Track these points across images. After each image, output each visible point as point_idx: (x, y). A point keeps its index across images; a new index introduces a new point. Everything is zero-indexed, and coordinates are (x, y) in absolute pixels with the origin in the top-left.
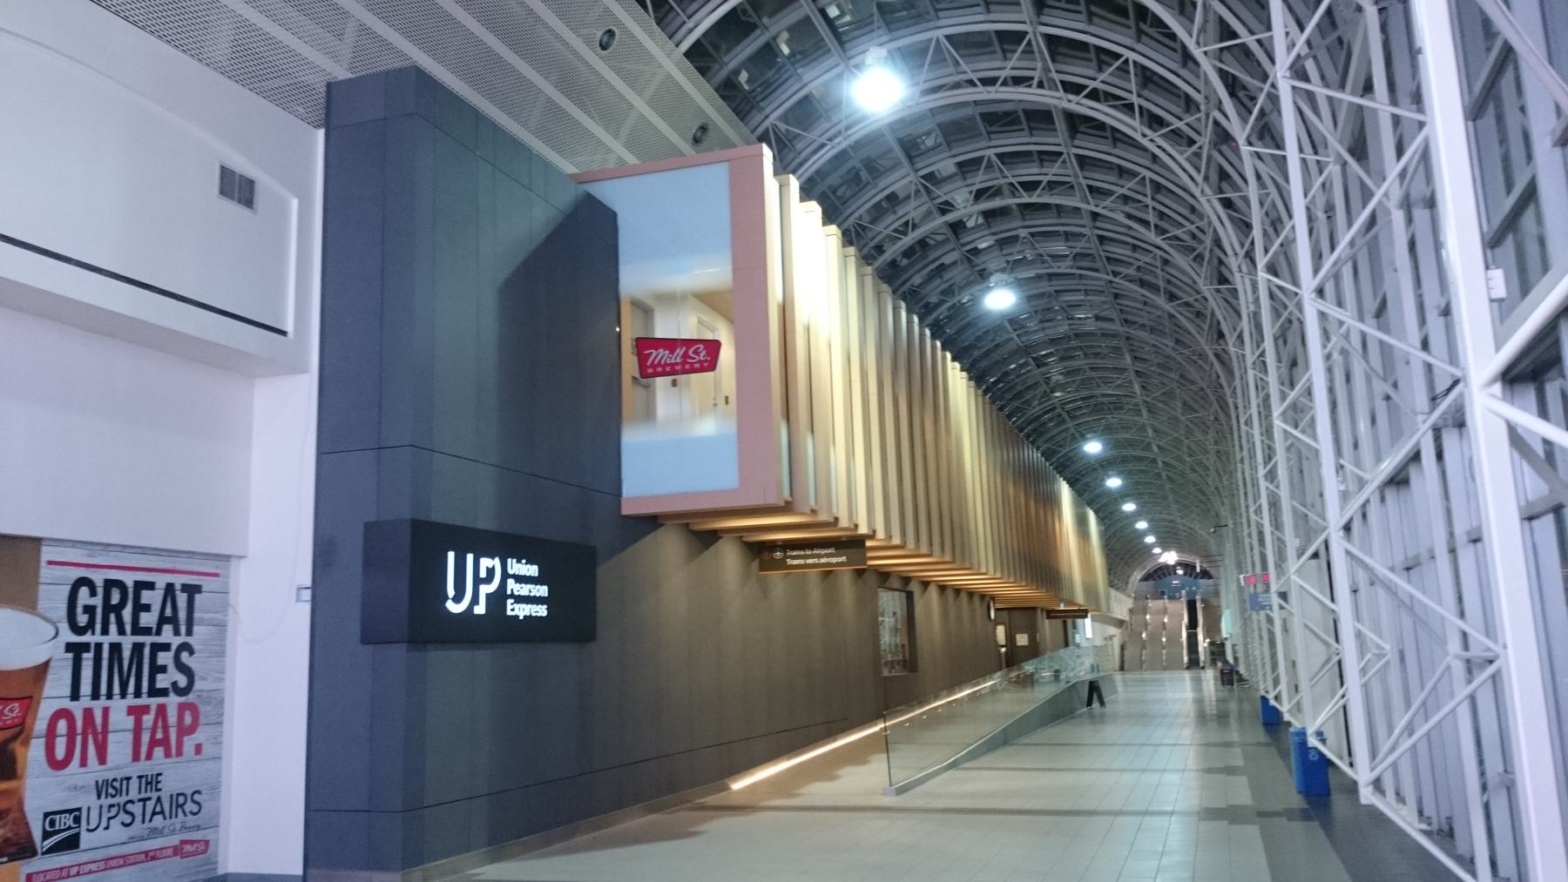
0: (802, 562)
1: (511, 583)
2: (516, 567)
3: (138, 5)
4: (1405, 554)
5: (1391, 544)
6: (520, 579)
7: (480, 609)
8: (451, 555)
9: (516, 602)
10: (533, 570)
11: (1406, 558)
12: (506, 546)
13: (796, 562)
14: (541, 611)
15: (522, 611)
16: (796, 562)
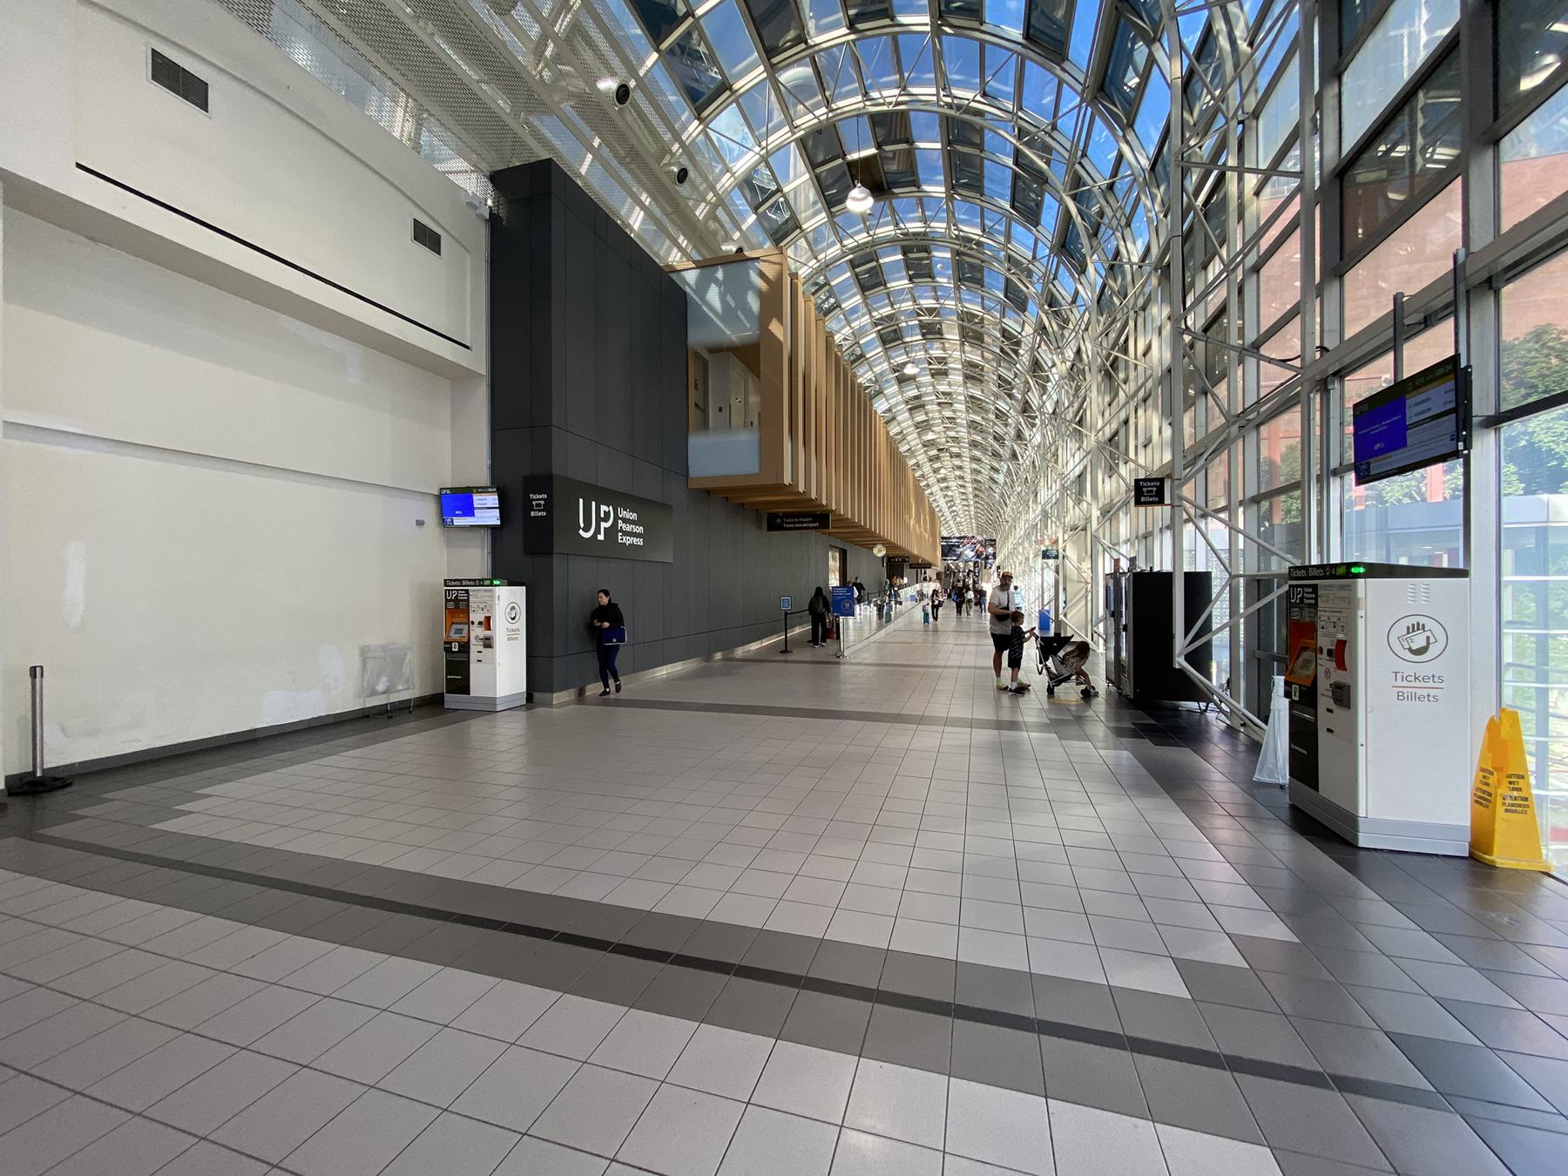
0: (792, 526)
1: (1305, 595)
2: (624, 514)
3: (262, 4)
4: (1496, 158)
5: (1458, 1096)
6: (1308, 593)
7: (601, 537)
8: (594, 503)
9: (624, 535)
10: (634, 516)
11: (1482, 440)
12: (616, 498)
13: (788, 526)
14: (639, 542)
15: (628, 540)
16: (788, 526)
